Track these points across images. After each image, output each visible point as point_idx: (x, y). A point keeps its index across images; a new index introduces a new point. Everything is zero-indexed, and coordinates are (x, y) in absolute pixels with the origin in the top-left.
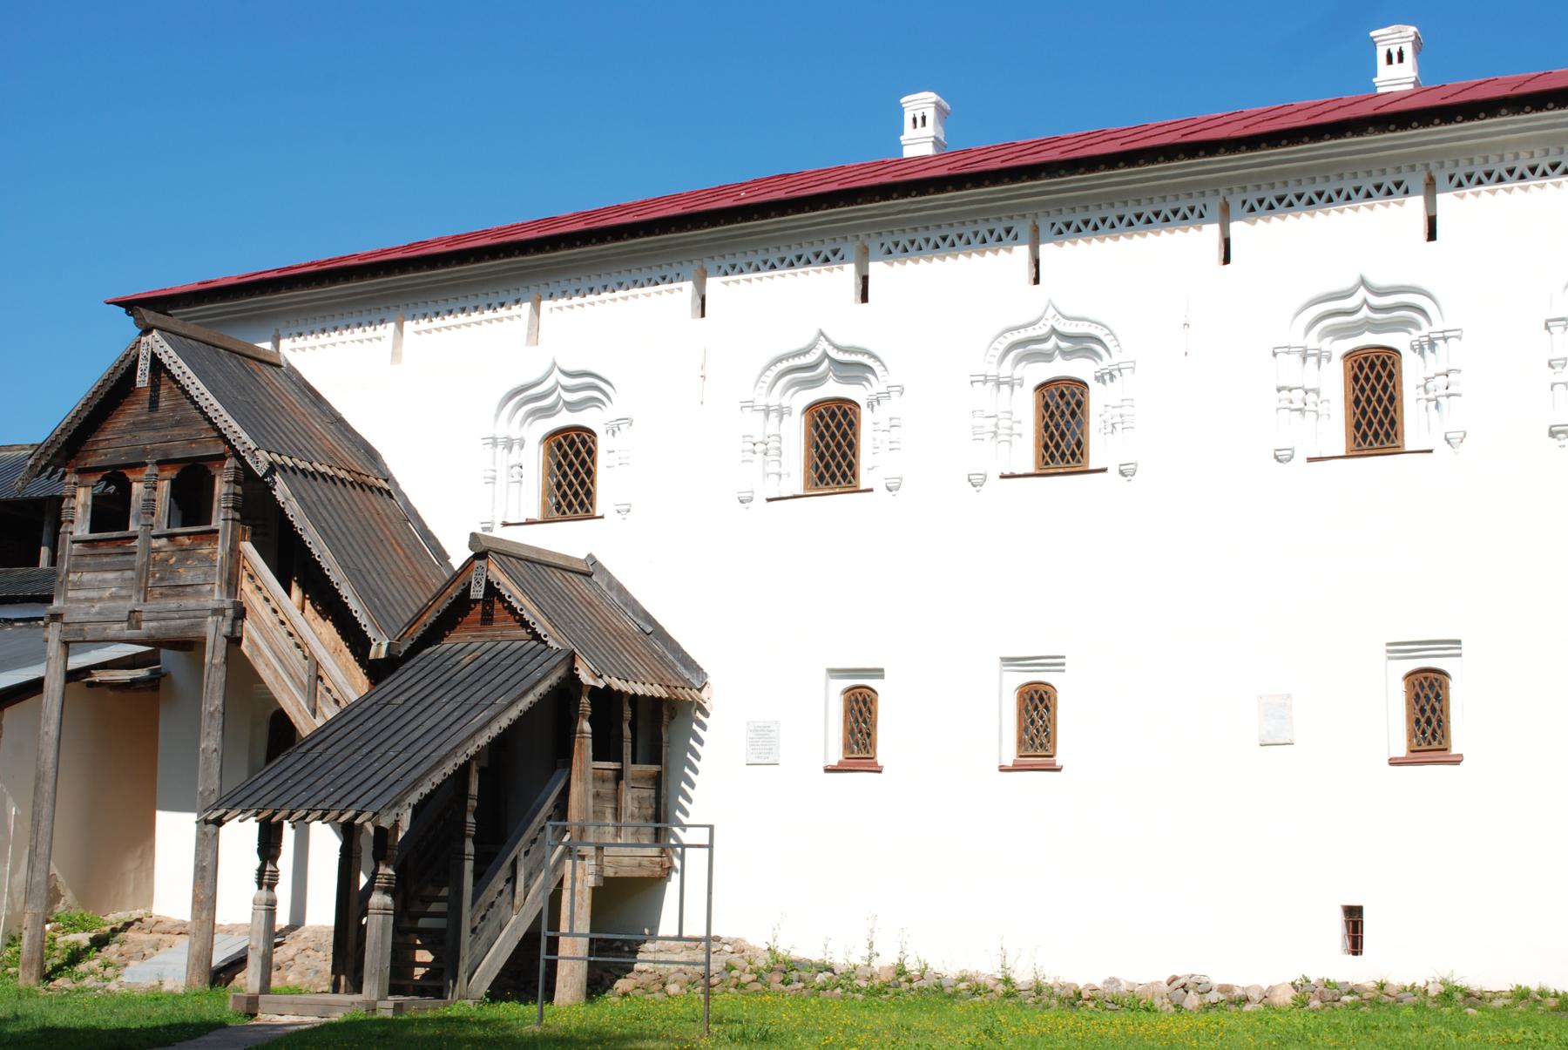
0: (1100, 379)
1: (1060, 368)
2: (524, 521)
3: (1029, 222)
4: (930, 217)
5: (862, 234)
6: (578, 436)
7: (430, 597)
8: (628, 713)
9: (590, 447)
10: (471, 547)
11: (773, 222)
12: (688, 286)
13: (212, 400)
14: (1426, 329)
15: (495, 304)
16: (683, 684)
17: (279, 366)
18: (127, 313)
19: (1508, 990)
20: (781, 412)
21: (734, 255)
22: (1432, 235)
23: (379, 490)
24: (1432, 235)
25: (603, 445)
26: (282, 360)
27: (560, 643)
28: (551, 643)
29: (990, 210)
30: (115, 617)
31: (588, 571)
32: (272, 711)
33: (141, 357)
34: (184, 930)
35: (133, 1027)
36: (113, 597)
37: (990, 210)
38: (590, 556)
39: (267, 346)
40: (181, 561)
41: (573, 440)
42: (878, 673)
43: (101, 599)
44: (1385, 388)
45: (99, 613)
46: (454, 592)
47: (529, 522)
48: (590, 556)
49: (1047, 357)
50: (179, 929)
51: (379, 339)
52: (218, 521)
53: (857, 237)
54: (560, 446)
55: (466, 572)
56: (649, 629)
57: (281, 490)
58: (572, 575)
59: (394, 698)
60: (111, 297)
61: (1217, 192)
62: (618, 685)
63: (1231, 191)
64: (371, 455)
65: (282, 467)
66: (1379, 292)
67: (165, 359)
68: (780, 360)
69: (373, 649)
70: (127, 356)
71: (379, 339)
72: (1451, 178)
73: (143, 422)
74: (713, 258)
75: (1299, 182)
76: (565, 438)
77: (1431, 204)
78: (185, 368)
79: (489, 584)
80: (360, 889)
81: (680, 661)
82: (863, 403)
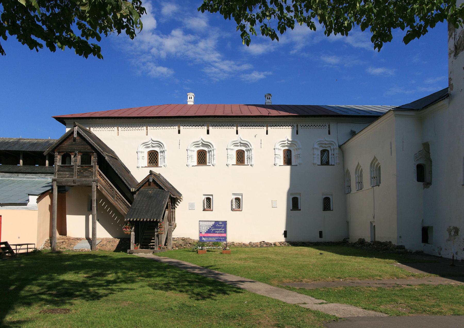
0: (160, 152)
1: (240, 148)
3: (236, 124)
4: (224, 121)
5: (208, 123)
11: (191, 119)
12: (206, 127)
14: (248, 148)
15: (285, 125)
19: (461, 260)
20: (193, 151)
22: (267, 134)
24: (267, 134)
28: (166, 190)
29: (231, 121)
30: (70, 181)
35: (16, 320)
36: (68, 177)
37: (231, 121)
39: (88, 128)
40: (84, 171)
42: (212, 195)
43: (65, 177)
44: (238, 156)
49: (238, 146)
50: (77, 239)
51: (113, 131)
52: (92, 164)
53: (207, 123)
60: (53, 116)
61: (266, 123)
63: (268, 123)
66: (204, 142)
67: (80, 132)
68: (195, 142)
70: (71, 131)
71: (113, 131)
72: (300, 125)
75: (191, 124)
77: (267, 128)
79: (153, 179)
82: (159, 152)
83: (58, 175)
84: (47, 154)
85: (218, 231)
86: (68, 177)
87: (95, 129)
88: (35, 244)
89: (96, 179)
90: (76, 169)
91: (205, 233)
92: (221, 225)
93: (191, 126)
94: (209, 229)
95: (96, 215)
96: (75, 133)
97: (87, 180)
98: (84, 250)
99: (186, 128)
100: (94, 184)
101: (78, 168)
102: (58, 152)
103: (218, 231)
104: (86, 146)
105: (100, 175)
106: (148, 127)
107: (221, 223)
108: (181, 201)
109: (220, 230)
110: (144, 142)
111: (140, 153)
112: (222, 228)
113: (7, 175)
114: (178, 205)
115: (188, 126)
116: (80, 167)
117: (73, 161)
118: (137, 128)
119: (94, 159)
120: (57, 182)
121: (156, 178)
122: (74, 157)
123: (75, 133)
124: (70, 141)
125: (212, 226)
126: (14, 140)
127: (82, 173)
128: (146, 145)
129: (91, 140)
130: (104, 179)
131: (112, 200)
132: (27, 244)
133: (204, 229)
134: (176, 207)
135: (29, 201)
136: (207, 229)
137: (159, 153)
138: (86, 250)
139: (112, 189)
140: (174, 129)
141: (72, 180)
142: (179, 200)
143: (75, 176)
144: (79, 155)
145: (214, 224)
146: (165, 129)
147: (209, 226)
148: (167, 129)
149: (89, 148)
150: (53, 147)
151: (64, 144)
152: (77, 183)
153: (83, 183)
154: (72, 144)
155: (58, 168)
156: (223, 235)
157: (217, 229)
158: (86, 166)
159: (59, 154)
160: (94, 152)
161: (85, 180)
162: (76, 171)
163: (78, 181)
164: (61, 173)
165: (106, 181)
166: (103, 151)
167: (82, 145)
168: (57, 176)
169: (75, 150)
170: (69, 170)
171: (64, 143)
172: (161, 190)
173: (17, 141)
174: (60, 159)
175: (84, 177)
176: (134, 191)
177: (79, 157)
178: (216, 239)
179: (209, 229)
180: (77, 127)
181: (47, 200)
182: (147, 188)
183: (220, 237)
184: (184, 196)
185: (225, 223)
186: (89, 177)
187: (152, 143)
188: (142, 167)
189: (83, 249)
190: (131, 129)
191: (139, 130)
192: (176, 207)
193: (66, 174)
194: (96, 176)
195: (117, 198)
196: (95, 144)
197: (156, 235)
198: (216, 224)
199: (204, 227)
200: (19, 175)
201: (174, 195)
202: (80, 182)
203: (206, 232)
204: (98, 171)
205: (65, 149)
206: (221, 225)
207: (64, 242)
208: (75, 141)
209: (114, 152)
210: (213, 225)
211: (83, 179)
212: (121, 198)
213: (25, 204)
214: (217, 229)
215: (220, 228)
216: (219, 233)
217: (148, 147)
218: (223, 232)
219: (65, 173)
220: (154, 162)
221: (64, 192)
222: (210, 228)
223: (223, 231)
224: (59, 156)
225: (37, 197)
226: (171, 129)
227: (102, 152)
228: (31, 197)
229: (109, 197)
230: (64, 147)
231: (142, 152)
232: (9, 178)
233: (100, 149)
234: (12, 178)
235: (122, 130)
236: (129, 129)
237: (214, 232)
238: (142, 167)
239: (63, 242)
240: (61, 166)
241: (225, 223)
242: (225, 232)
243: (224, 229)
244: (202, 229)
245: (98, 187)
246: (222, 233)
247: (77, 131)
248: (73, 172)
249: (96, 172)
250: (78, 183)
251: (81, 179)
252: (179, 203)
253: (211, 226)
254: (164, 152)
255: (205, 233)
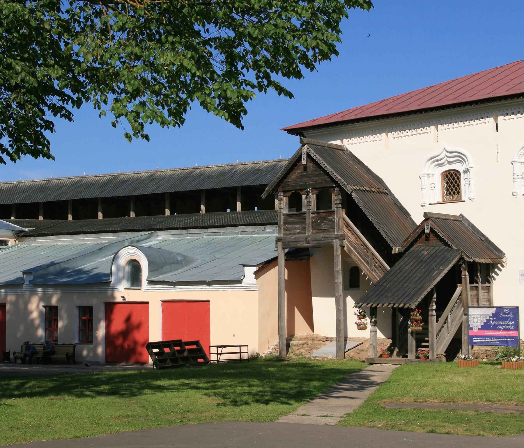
2: (436, 203)
6: (454, 173)
7: (411, 232)
8: (479, 268)
9: (458, 177)
10: (424, 216)
13: (330, 168)
16: (497, 258)
17: (344, 150)
18: (288, 133)
21: (507, 110)
23: (385, 193)
25: (463, 176)
26: (345, 148)
27: (457, 248)
28: (454, 247)
30: (301, 240)
31: (461, 219)
32: (350, 268)
33: (303, 154)
34: (327, 340)
36: (299, 233)
38: (461, 215)
40: (322, 222)
41: (452, 174)
43: (294, 234)
45: (295, 239)
46: (419, 231)
47: (438, 203)
48: (461, 215)
50: (325, 339)
51: (380, 140)
52: (334, 208)
54: (447, 176)
55: (423, 225)
56: (483, 239)
57: (354, 195)
58: (456, 222)
59: (405, 267)
60: (282, 128)
62: (477, 260)
64: (379, 181)
65: (355, 190)
67: (312, 155)
69: (393, 250)
70: (298, 153)
71: (380, 140)
73: (305, 175)
74: (500, 111)
76: (449, 174)
78: (319, 157)
79: (431, 228)
80: (295, 307)
81: (494, 249)
83: (285, 230)
84: (266, 196)
85: (502, 325)
86: (299, 233)
87: (351, 141)
88: (247, 346)
89: (340, 233)
90: (310, 218)
91: (479, 329)
92: (508, 314)
93: (519, 113)
94: (485, 321)
95: (342, 297)
96: (304, 157)
97: (327, 236)
98: (326, 358)
99: (509, 119)
100: (336, 243)
101: (313, 216)
102: (283, 192)
103: (502, 325)
104: (323, 178)
105: (348, 226)
106: (439, 126)
107: (507, 311)
108: (503, 266)
109: (506, 323)
110: (432, 156)
111: (426, 178)
112: (510, 321)
113: (249, 229)
114: (497, 275)
115: (513, 114)
116: (316, 215)
117: (306, 205)
118: (419, 131)
119: (336, 198)
120: (283, 242)
121: (436, 227)
122: (306, 198)
123: (304, 157)
124: (299, 171)
125: (491, 315)
126: (269, 164)
127: (319, 224)
128: (435, 160)
129: (328, 167)
130: (354, 233)
131: (368, 269)
132: (240, 346)
133: (477, 322)
134: (495, 279)
135: (244, 277)
136: (481, 321)
137: (462, 174)
138: (330, 357)
139: (367, 249)
140: (485, 123)
141: (304, 237)
142: (499, 265)
143: (309, 230)
144: (314, 194)
145: (494, 313)
146: (469, 125)
147: (486, 316)
148: (472, 125)
149: (328, 180)
150: (273, 184)
151: (291, 177)
152: (311, 242)
153: (320, 242)
154: (302, 176)
155: (285, 219)
156: (512, 333)
157: (501, 322)
158: (324, 212)
159: (286, 195)
160: (335, 187)
161: (323, 237)
162: (309, 222)
163: (313, 239)
164: (289, 226)
165: (356, 236)
166: (346, 184)
167: (317, 176)
168: (283, 232)
169: (306, 185)
170: (300, 220)
171: (291, 175)
172: (447, 248)
173: (275, 165)
174: (286, 203)
175: (322, 232)
176: (397, 252)
177: (313, 198)
178: (498, 341)
179: (485, 321)
180: (306, 146)
181: (272, 274)
182: (423, 246)
183: (506, 337)
184: (508, 259)
185: (515, 310)
186: (330, 232)
187: (446, 156)
188: (430, 204)
189: (326, 356)
190: (409, 132)
191: (424, 133)
192: (495, 279)
193: (295, 229)
194: (339, 229)
195: (375, 266)
196: (334, 172)
197: (409, 334)
198: (499, 313)
199: (477, 318)
200: (266, 229)
201: (468, 257)
202: (316, 241)
203: (480, 327)
204: (344, 220)
205: (292, 186)
206: (508, 314)
207: (305, 343)
208: (307, 170)
209: (381, 179)
210: (493, 314)
211: (321, 235)
212: (381, 266)
213: (239, 281)
214: (501, 322)
215: (506, 319)
216: (504, 330)
217: (441, 165)
218: (513, 328)
219: (294, 226)
220: (454, 193)
221: (306, 257)
222: (487, 320)
223: (512, 325)
224: (285, 198)
225: (255, 269)
226: (481, 123)
227: (346, 187)
228: (246, 268)
229: (362, 265)
230: (290, 183)
231: (429, 176)
232: (252, 234)
233: (342, 180)
234: (255, 234)
235: (394, 138)
236: (405, 133)
237: (495, 328)
238: (430, 204)
239: (303, 344)
240: (288, 215)
241: (515, 310)
242: (516, 327)
243: (513, 323)
244: (474, 322)
245: (345, 248)
246: (509, 330)
247: (307, 153)
248: (306, 224)
249: (340, 222)
250: (313, 242)
251: (317, 235)
252: (500, 270)
253: (490, 317)
254: (469, 172)
255: (479, 329)
